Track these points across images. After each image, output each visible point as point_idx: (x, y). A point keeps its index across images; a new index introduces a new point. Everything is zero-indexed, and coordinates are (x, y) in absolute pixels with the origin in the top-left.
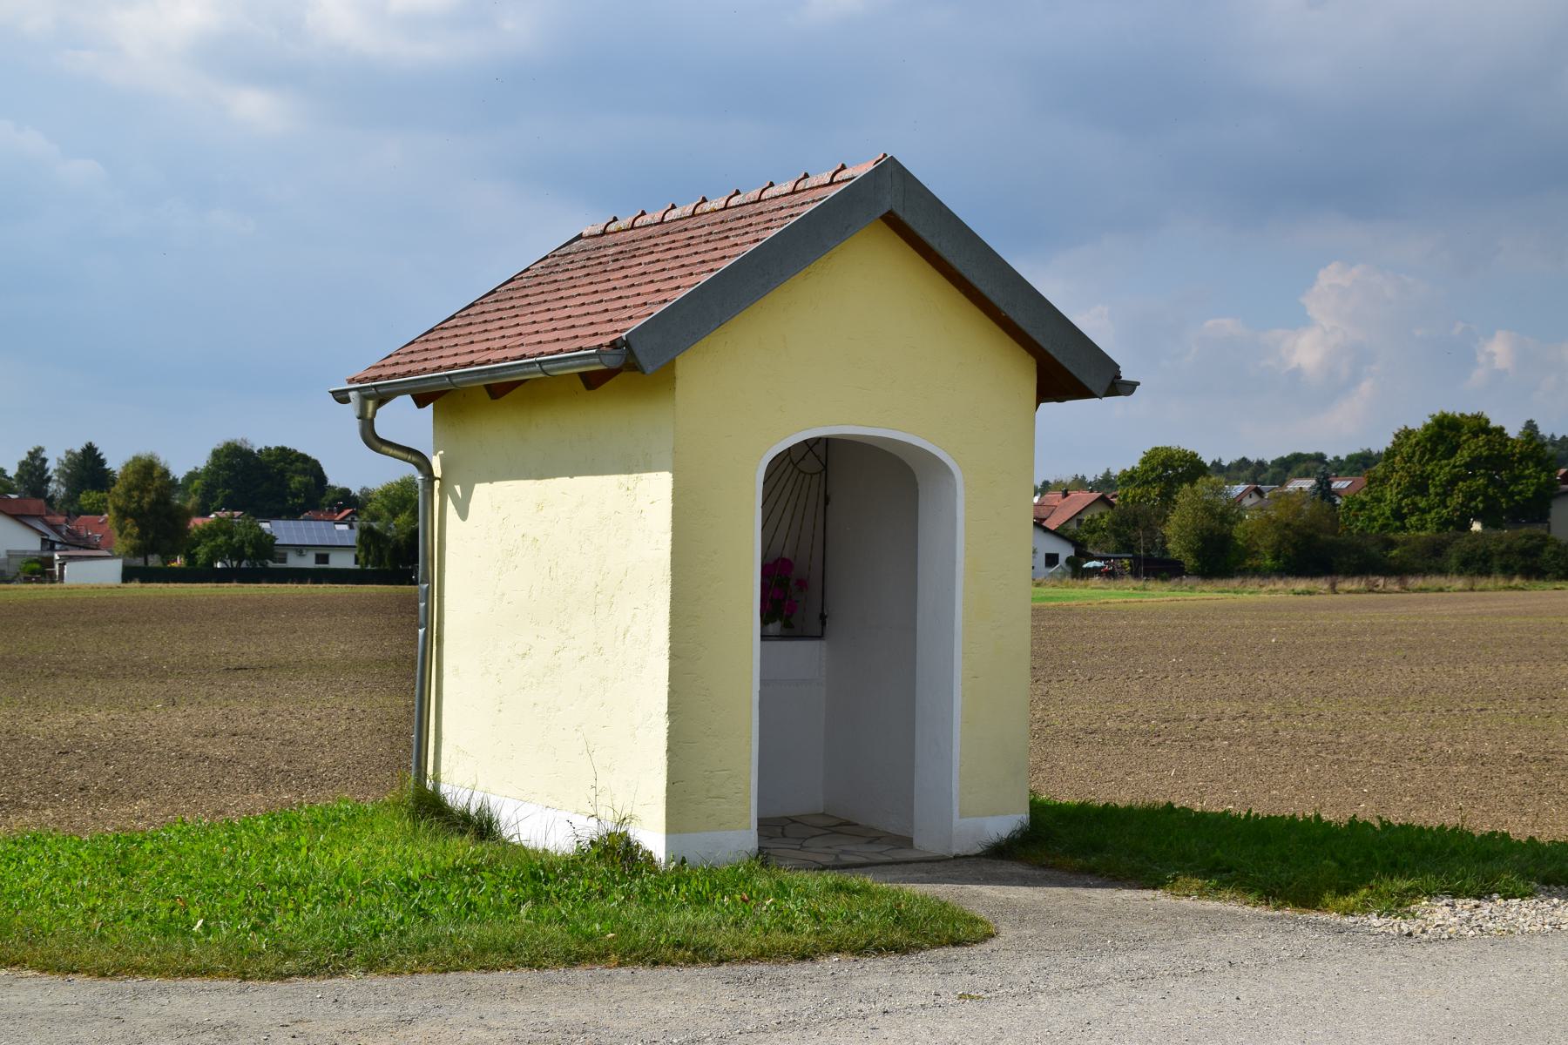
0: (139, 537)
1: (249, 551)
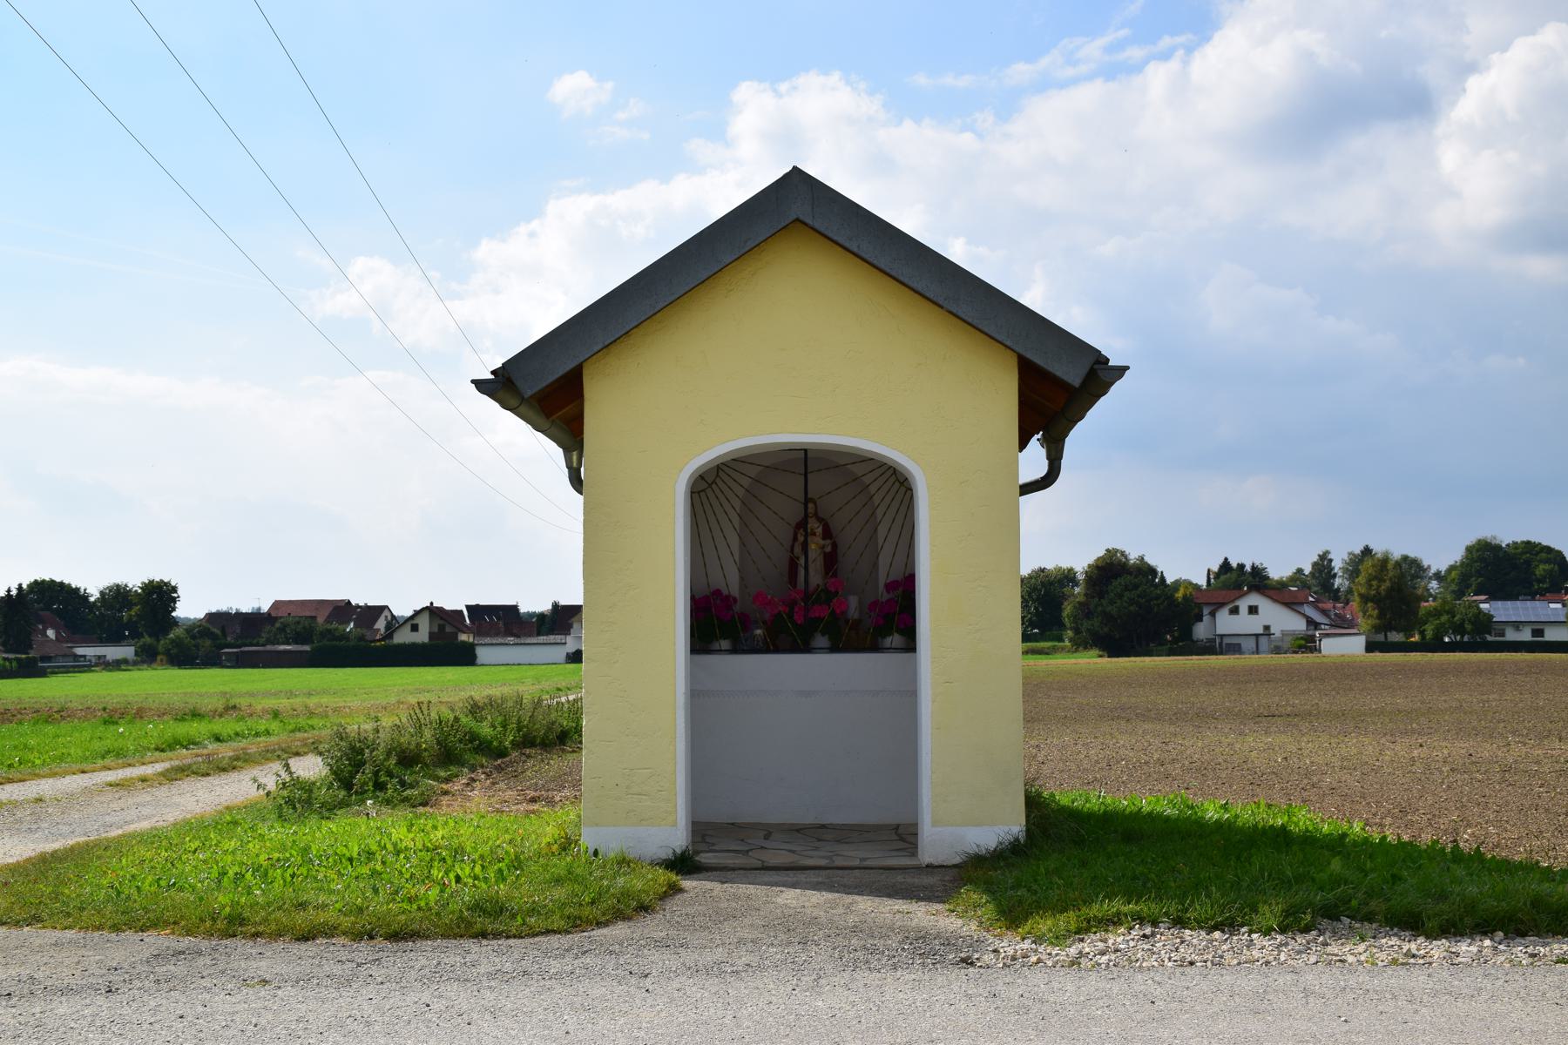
0: (1380, 617)
1: (1468, 627)
